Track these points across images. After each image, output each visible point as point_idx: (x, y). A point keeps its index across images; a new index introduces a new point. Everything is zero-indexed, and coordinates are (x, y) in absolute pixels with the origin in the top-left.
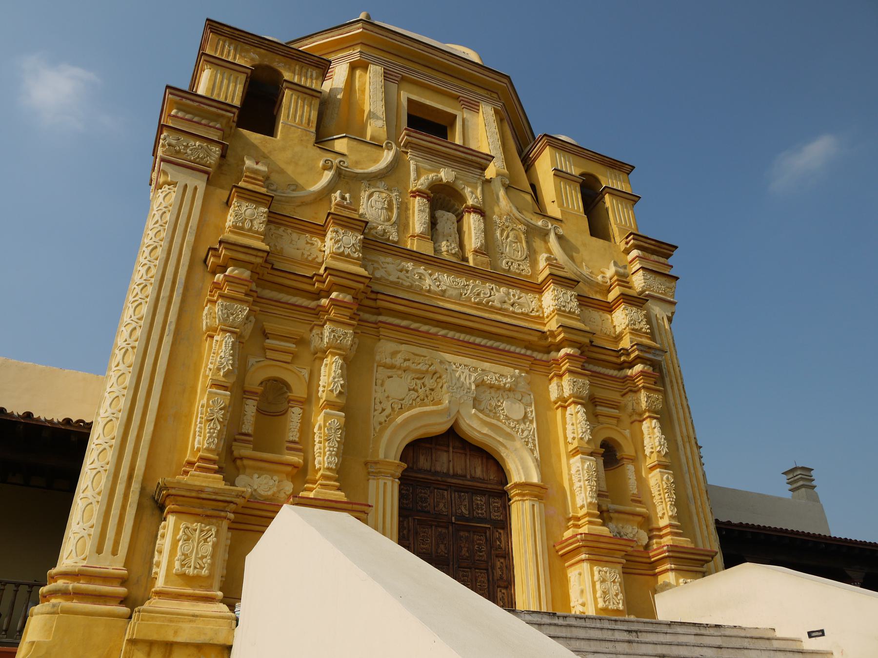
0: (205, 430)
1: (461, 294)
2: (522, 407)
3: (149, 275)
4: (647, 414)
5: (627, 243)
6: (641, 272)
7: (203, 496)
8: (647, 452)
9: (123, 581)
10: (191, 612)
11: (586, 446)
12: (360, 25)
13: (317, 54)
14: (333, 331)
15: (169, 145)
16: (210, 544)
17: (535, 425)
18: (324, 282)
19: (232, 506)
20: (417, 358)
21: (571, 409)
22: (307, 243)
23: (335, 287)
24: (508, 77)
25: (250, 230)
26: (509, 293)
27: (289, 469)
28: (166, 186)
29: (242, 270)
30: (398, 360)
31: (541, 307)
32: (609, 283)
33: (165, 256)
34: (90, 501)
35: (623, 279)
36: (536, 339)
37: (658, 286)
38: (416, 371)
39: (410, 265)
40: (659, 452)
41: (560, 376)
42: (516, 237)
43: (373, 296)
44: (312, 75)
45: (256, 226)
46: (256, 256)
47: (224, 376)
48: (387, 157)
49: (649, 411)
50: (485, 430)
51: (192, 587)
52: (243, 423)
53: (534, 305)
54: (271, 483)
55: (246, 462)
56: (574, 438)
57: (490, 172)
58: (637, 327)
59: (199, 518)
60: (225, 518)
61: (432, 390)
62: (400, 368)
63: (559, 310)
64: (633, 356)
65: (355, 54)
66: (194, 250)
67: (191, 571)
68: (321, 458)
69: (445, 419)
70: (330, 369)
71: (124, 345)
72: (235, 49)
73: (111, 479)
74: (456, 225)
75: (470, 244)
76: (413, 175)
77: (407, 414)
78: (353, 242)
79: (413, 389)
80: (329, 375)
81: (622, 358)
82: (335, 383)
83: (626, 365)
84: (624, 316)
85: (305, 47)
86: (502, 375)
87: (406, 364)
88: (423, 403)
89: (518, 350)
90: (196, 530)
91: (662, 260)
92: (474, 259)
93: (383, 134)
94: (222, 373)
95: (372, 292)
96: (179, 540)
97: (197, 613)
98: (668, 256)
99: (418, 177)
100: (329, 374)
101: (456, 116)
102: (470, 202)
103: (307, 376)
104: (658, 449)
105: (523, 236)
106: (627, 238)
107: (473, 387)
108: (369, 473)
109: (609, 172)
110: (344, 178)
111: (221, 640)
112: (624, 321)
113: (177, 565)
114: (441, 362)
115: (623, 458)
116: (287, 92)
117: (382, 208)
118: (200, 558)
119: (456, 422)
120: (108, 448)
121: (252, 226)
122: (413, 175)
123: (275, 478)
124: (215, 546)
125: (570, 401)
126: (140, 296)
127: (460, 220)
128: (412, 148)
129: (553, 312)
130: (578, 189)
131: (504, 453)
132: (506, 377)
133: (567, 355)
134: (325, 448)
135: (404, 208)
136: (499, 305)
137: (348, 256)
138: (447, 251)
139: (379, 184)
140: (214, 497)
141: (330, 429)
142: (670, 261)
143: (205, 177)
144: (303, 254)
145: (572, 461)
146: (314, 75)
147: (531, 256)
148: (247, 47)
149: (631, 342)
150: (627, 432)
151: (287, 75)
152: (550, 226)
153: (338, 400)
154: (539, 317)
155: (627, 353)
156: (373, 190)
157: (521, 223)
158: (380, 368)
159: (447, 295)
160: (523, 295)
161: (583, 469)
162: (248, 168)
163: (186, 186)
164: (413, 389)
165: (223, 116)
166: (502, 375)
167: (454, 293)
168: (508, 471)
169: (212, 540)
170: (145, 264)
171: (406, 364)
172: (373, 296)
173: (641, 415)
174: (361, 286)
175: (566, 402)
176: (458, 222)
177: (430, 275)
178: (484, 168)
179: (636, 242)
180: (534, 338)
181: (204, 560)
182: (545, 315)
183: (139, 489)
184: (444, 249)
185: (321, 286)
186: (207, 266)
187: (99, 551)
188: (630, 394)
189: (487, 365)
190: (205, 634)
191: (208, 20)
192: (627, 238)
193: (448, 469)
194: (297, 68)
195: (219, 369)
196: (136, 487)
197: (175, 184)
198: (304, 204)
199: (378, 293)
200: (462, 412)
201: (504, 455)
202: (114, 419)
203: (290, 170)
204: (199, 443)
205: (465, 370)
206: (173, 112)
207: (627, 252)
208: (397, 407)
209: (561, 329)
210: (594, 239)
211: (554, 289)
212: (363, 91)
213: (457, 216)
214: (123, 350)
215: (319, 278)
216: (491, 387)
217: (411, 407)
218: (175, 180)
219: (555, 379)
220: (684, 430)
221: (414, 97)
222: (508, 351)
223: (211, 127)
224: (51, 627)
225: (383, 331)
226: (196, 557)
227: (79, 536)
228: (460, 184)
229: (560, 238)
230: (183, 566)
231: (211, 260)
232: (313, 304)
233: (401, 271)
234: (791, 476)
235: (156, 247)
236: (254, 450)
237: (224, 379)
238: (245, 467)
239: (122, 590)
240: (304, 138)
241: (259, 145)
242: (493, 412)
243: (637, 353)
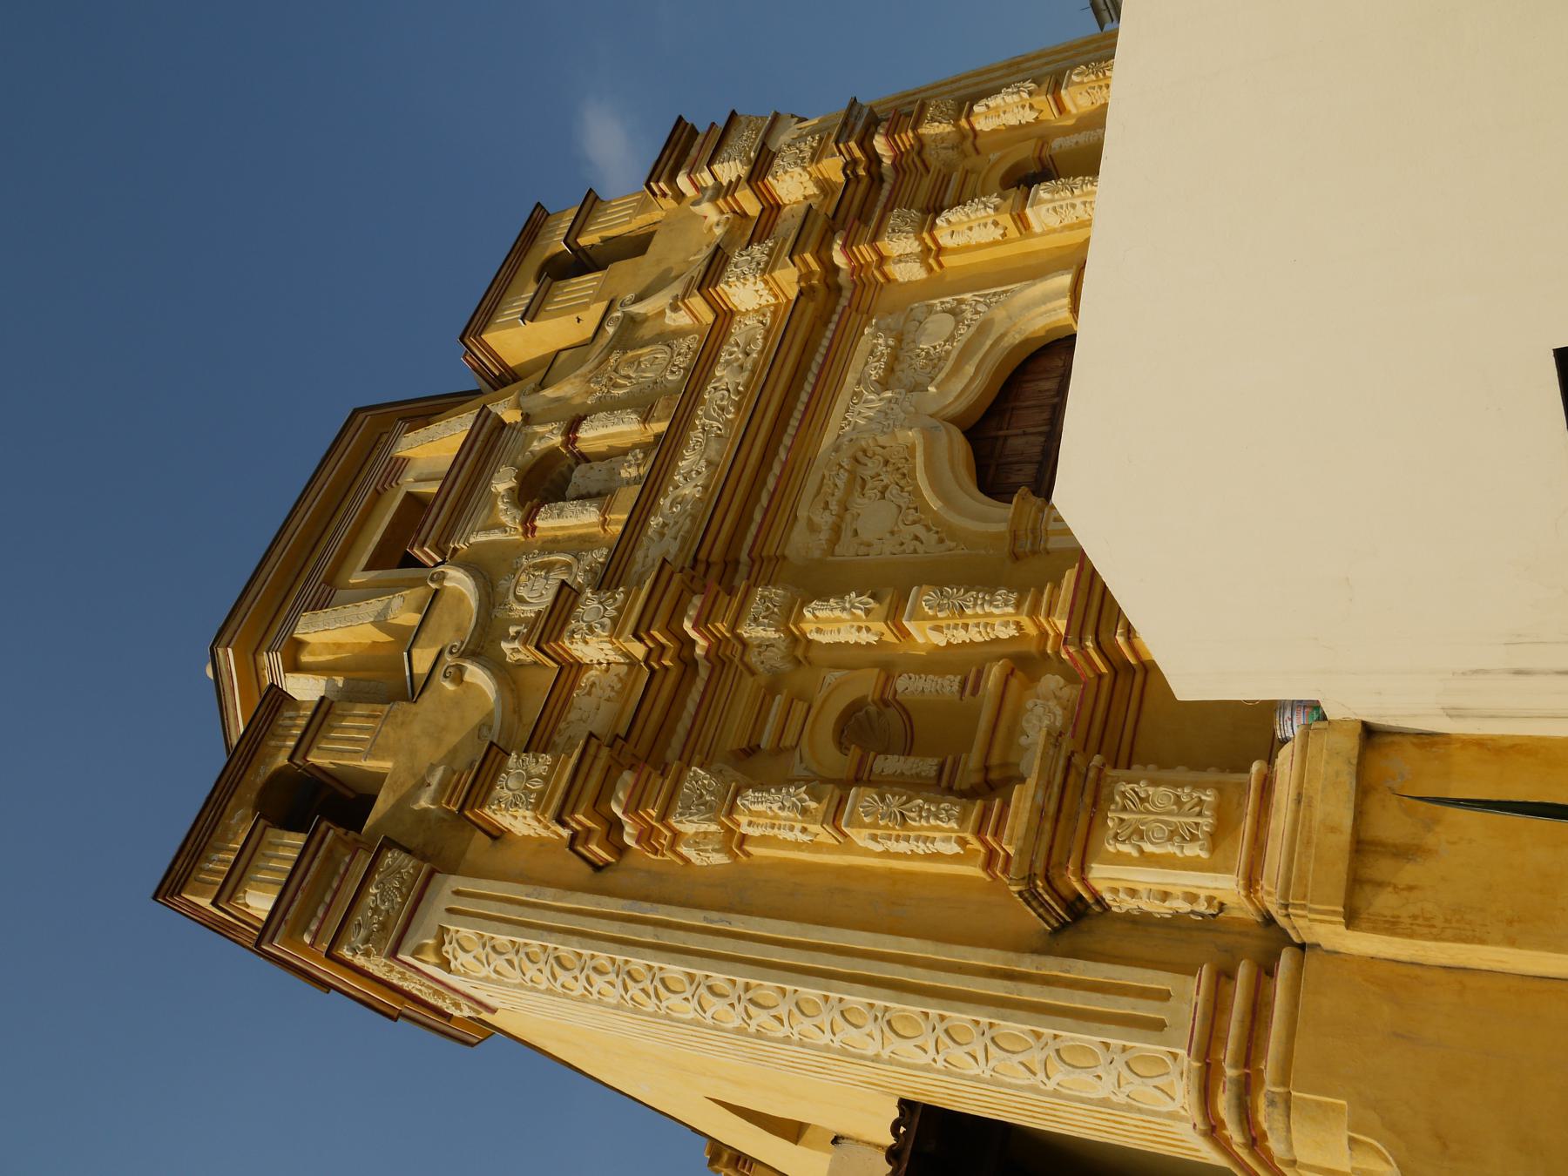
0: (921, 828)
1: (719, 436)
2: (933, 317)
3: (610, 968)
4: (963, 122)
5: (664, 195)
6: (716, 167)
7: (1052, 808)
8: (1030, 116)
9: (1224, 975)
10: (1291, 806)
11: (1010, 201)
12: (220, 651)
13: (257, 700)
14: (755, 620)
15: (366, 941)
16: (1151, 790)
17: (968, 296)
18: (663, 647)
19: (1077, 759)
20: (825, 489)
21: (945, 240)
22: (589, 693)
23: (674, 626)
24: (356, 412)
25: (546, 779)
26: (728, 363)
27: (1014, 682)
28: (446, 947)
29: (618, 785)
30: (824, 520)
31: (756, 311)
32: (730, 215)
33: (575, 938)
34: (1053, 1054)
35: (722, 192)
36: (811, 306)
37: (745, 141)
38: (849, 490)
39: (655, 522)
40: (1030, 94)
41: (882, 259)
42: (630, 363)
43: (701, 568)
44: (291, 718)
45: (542, 769)
46: (595, 757)
47: (818, 800)
48: (458, 581)
49: (957, 120)
50: (970, 369)
51: (1239, 822)
52: (918, 775)
53: (751, 322)
54: (1039, 710)
55: (995, 760)
56: (996, 224)
57: (511, 416)
58: (808, 154)
59: (1098, 821)
60: (1100, 770)
61: (886, 463)
62: (840, 517)
63: (764, 271)
64: (858, 153)
65: (271, 663)
66: (572, 887)
67: (1206, 822)
68: (997, 622)
69: (944, 439)
70: (827, 620)
71: (739, 1008)
72: (219, 850)
73: (1008, 1012)
74: (595, 464)
75: (632, 432)
76: (496, 536)
77: (927, 493)
78: (595, 604)
79: (883, 493)
80: (838, 624)
81: (862, 172)
82: (853, 606)
83: (873, 169)
84: (787, 177)
85: (239, 726)
86: (872, 353)
87: (834, 507)
88: (908, 475)
89: (829, 334)
90: (1122, 820)
91: (700, 139)
92: (659, 420)
93: (415, 594)
94: (813, 805)
95: (693, 568)
96: (1141, 851)
97: (1293, 795)
98: (694, 132)
99: (502, 527)
100: (838, 620)
101: (409, 495)
102: (557, 440)
103: (837, 674)
104: (1025, 95)
105: (630, 354)
106: (654, 194)
107: (888, 394)
108: (1034, 552)
109: (541, 242)
110: (481, 647)
111: (1350, 744)
112: (796, 176)
113: (1193, 851)
114: (837, 449)
115: (1040, 158)
116: (316, 759)
117: (546, 578)
118: (1180, 808)
119: (955, 421)
120: (945, 1025)
121: (540, 776)
122: (496, 536)
123: (1030, 704)
124: (1154, 783)
125: (931, 261)
126: (646, 984)
127: (583, 458)
128: (447, 541)
129: (766, 282)
130: (562, 283)
131: (1015, 338)
132: (875, 346)
133: (844, 246)
134: (976, 616)
135: (553, 545)
136: (746, 374)
137: (620, 610)
138: (638, 466)
139: (501, 589)
140: (1056, 789)
141: (941, 608)
142: (702, 128)
143: (438, 876)
144: (609, 700)
145: (1037, 228)
146: (292, 714)
147: (667, 338)
148: (219, 831)
149: (833, 155)
150: (993, 157)
151: (282, 760)
152: (619, 314)
153: (888, 600)
154: (774, 313)
155: (850, 165)
156: (511, 597)
157: (607, 359)
158: (838, 549)
159: (717, 459)
160: (732, 340)
161: (1052, 201)
162: (434, 801)
163: (449, 911)
164: (883, 493)
165: (330, 851)
166: (872, 353)
167: (714, 445)
168: (1050, 331)
169: (1143, 789)
170: (588, 979)
171: (834, 507)
172: (701, 568)
173: (964, 137)
174: (677, 577)
175: (930, 250)
176: (588, 461)
177: (677, 487)
178: (502, 425)
179: (664, 177)
180: (810, 309)
181: (1184, 799)
182: (772, 300)
183: (1035, 957)
184: (633, 472)
185: (670, 653)
186: (608, 864)
187: (1159, 1025)
188: (926, 155)
189: (851, 378)
190: (1337, 774)
191: (155, 898)
192: (654, 194)
193: (1040, 433)
194: (273, 743)
195: (805, 811)
196: (1027, 964)
197: (443, 931)
198: (518, 711)
199: (695, 559)
200: (933, 408)
201: (1018, 338)
202: (887, 1016)
203: (452, 739)
204: (947, 840)
205: (858, 409)
206: (307, 939)
207: (680, 196)
208: (912, 515)
209: (796, 258)
210: (650, 249)
211: (727, 283)
212: (339, 646)
213: (577, 464)
214: (751, 1009)
215: (655, 655)
216: (890, 369)
217: (917, 492)
218: (435, 930)
219: (886, 268)
220: (998, 74)
221: (364, 560)
222: (829, 349)
223: (347, 870)
224: (1319, 1104)
225: (770, 550)
226: (1178, 815)
227: (1126, 1073)
228: (525, 459)
229: (639, 298)
230: (1194, 838)
231: (597, 851)
232: (703, 673)
233: (662, 535)
234: (1106, 14)
235: (557, 959)
236: (969, 750)
237: (825, 801)
238: (1005, 765)
239: (1243, 972)
240: (400, 719)
241: (398, 795)
242: (934, 362)
243: (852, 144)
